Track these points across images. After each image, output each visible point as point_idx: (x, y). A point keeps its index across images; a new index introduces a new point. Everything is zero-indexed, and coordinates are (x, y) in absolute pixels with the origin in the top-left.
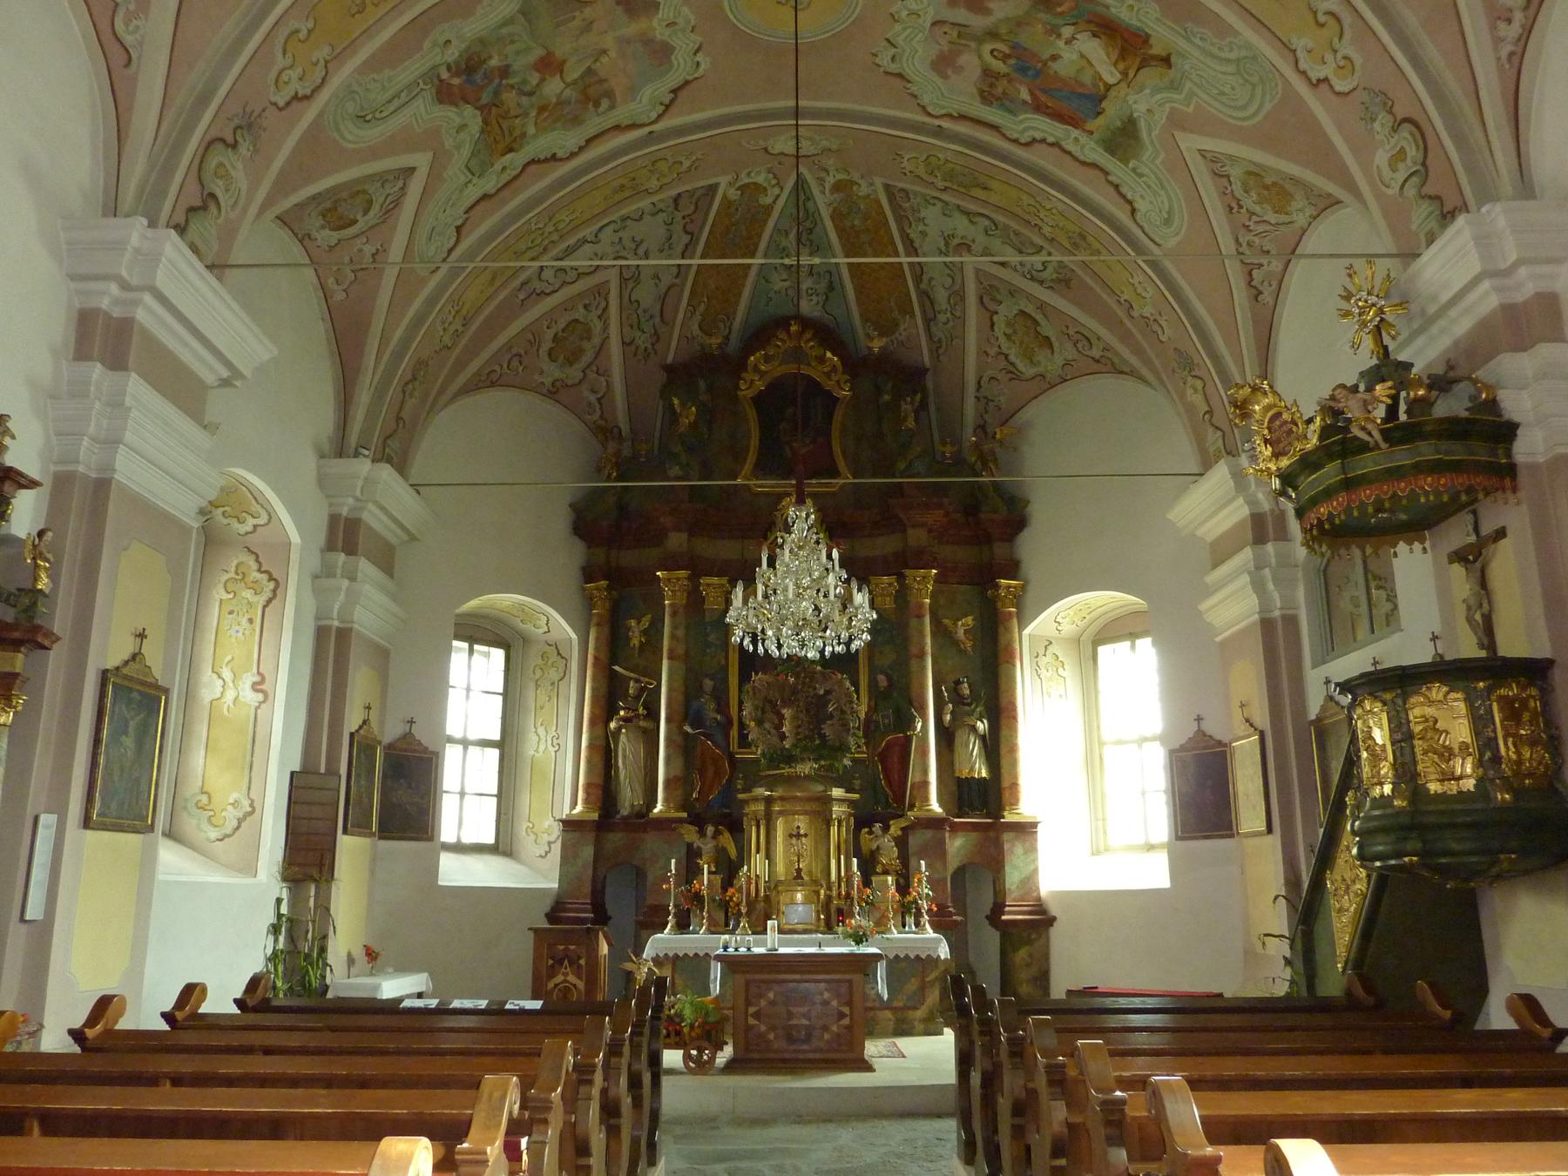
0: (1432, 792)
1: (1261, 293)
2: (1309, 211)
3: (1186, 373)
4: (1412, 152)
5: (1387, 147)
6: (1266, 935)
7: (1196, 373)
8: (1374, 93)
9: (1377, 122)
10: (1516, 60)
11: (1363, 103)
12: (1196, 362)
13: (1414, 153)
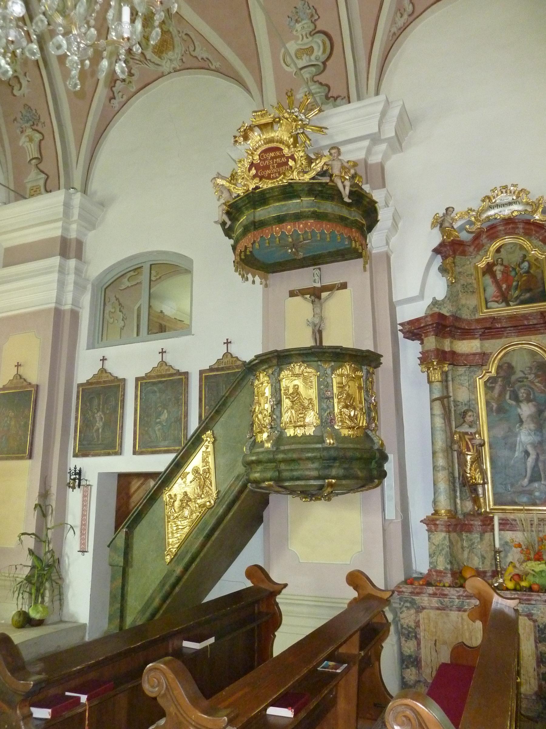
0: (343, 435)
1: (114, 98)
2: (176, 64)
3: (28, 125)
4: (319, 53)
5: (300, 42)
6: (23, 534)
7: (39, 128)
8: (308, 5)
9: (300, 24)
10: (395, 37)
11: (295, 8)
12: (42, 120)
13: (320, 53)
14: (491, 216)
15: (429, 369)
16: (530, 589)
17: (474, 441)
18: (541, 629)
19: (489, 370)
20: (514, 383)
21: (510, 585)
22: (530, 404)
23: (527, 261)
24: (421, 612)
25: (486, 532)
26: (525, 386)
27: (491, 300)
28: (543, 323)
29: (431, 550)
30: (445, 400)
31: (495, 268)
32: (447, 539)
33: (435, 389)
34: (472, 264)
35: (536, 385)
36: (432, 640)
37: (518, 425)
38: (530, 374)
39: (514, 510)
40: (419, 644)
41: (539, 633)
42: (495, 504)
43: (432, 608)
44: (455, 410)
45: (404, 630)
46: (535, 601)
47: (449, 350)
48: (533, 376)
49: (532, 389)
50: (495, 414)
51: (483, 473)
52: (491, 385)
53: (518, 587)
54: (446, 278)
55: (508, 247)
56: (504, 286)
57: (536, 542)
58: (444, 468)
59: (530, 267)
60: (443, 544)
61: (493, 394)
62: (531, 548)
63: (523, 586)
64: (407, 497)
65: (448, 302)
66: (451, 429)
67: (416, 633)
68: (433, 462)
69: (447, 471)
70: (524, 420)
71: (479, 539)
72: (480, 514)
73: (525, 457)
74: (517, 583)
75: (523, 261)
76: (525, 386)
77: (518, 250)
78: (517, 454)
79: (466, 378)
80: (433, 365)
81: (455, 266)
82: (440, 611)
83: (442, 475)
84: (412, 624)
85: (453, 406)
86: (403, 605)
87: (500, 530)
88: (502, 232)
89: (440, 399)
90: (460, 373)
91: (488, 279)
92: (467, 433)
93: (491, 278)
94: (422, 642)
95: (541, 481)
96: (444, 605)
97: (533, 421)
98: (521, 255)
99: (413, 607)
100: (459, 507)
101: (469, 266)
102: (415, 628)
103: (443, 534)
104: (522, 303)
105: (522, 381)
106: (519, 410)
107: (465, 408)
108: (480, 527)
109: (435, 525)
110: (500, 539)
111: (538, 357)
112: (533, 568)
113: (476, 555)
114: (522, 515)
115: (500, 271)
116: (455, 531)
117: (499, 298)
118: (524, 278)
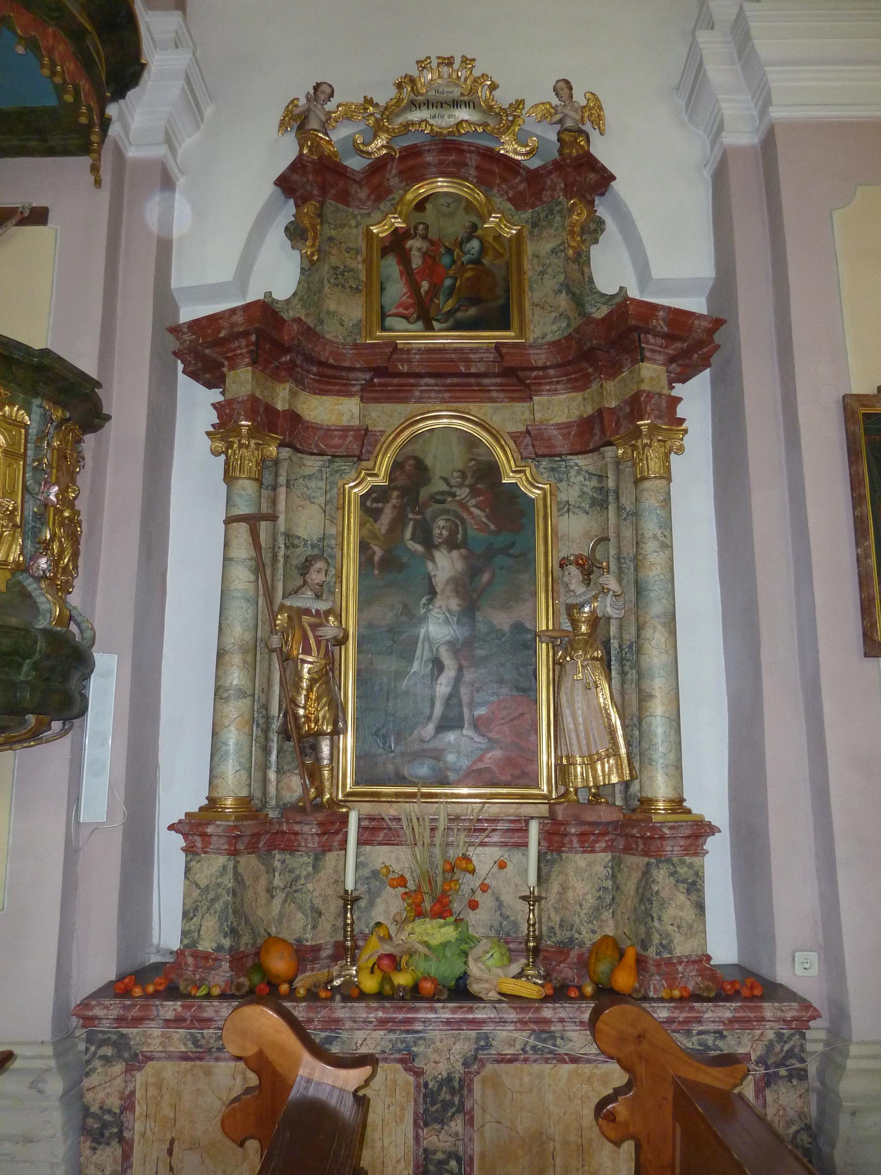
14: (413, 124)
15: (230, 446)
16: (415, 993)
17: (322, 631)
18: (432, 1092)
19: (374, 469)
20: (426, 505)
21: (370, 984)
22: (455, 554)
23: (478, 238)
24: (139, 1069)
25: (330, 850)
26: (447, 512)
27: (394, 311)
28: (498, 375)
29: (189, 901)
30: (264, 525)
31: (409, 243)
32: (230, 871)
33: (241, 496)
34: (360, 228)
35: (470, 513)
36: (162, 1141)
37: (424, 600)
38: (461, 485)
39: (398, 795)
40: (127, 1156)
41: (425, 1102)
42: (356, 783)
43: (169, 1057)
44: (286, 557)
45: (90, 1121)
46: (424, 1022)
47: (287, 408)
48: (467, 490)
49: (462, 519)
50: (376, 572)
51: (337, 709)
52: (375, 505)
53: (387, 988)
54: (301, 251)
55: (442, 201)
56: (425, 285)
57: (440, 870)
58: (242, 693)
59: (483, 250)
60: (219, 885)
61: (377, 526)
62: (425, 888)
63: (399, 986)
64: (157, 765)
65: (299, 306)
66: (269, 596)
67: (121, 1127)
68: (217, 678)
69: (248, 701)
70: (438, 590)
71: (310, 869)
72: (318, 807)
73: (432, 674)
74: (386, 979)
75: (470, 238)
76: (447, 512)
77: (461, 213)
78: (416, 666)
79: (322, 484)
80: (239, 435)
81: (322, 223)
82: (190, 1064)
83: (235, 709)
84: (115, 1103)
85: (283, 546)
86: (94, 1054)
87: (360, 843)
88: (434, 170)
89: (252, 520)
90: (308, 471)
91: (391, 266)
92: (307, 612)
93: (399, 263)
94: (137, 1148)
95: (462, 727)
96: (201, 1046)
97: (457, 592)
98: (467, 224)
99: (121, 1057)
100: (272, 790)
101: (355, 231)
102: (122, 1113)
103: (222, 860)
104: (457, 327)
105: (443, 502)
106: (430, 566)
107: (309, 552)
108: (316, 838)
109: (204, 836)
110: (358, 866)
111: (481, 451)
112: (425, 939)
113: (300, 908)
114: (413, 808)
115: (420, 249)
116: (252, 848)
117: (411, 310)
118: (468, 274)
